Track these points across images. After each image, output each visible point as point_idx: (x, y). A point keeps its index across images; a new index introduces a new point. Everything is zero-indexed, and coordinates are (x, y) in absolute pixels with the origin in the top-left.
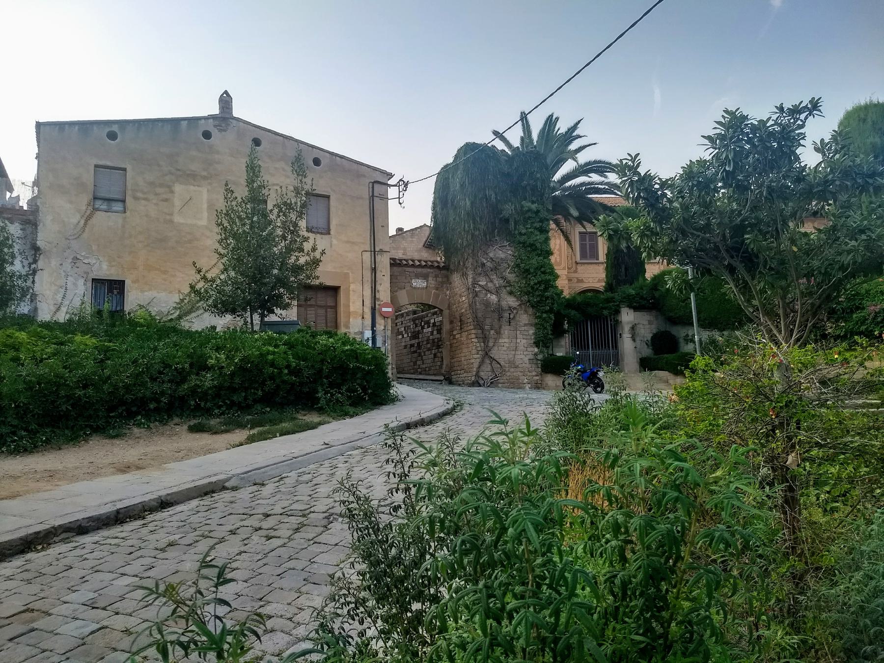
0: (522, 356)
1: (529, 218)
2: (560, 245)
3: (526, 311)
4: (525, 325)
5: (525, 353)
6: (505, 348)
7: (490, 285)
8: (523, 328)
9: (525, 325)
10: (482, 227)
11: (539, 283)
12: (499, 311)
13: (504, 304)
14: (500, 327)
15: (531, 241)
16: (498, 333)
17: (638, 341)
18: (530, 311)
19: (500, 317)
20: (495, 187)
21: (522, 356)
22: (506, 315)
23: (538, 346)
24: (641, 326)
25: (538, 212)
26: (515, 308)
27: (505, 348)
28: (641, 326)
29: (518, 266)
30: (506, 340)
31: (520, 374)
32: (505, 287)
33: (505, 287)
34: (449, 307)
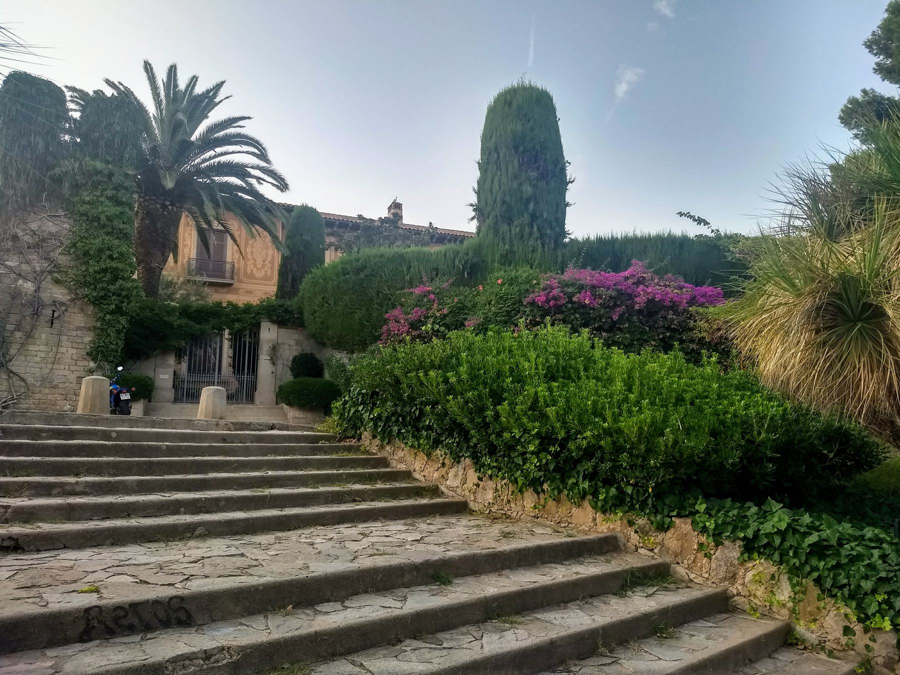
0: (66, 373)
1: (99, 182)
2: (273, 257)
3: (82, 310)
4: (79, 328)
5: (72, 368)
6: (38, 359)
7: (24, 267)
8: (74, 333)
9: (79, 328)
10: (21, 185)
11: (105, 271)
12: (36, 307)
13: (45, 296)
14: (33, 327)
15: (93, 212)
16: (29, 336)
17: (280, 367)
18: (90, 309)
19: (36, 314)
20: (47, 133)
21: (66, 373)
22: (48, 312)
23: (94, 359)
24: (286, 346)
25: (111, 175)
26: (62, 304)
27: (38, 359)
28: (286, 346)
29: (74, 245)
30: (42, 348)
31: (59, 397)
32: (50, 272)
33: (50, 272)
34: (517, 366)
